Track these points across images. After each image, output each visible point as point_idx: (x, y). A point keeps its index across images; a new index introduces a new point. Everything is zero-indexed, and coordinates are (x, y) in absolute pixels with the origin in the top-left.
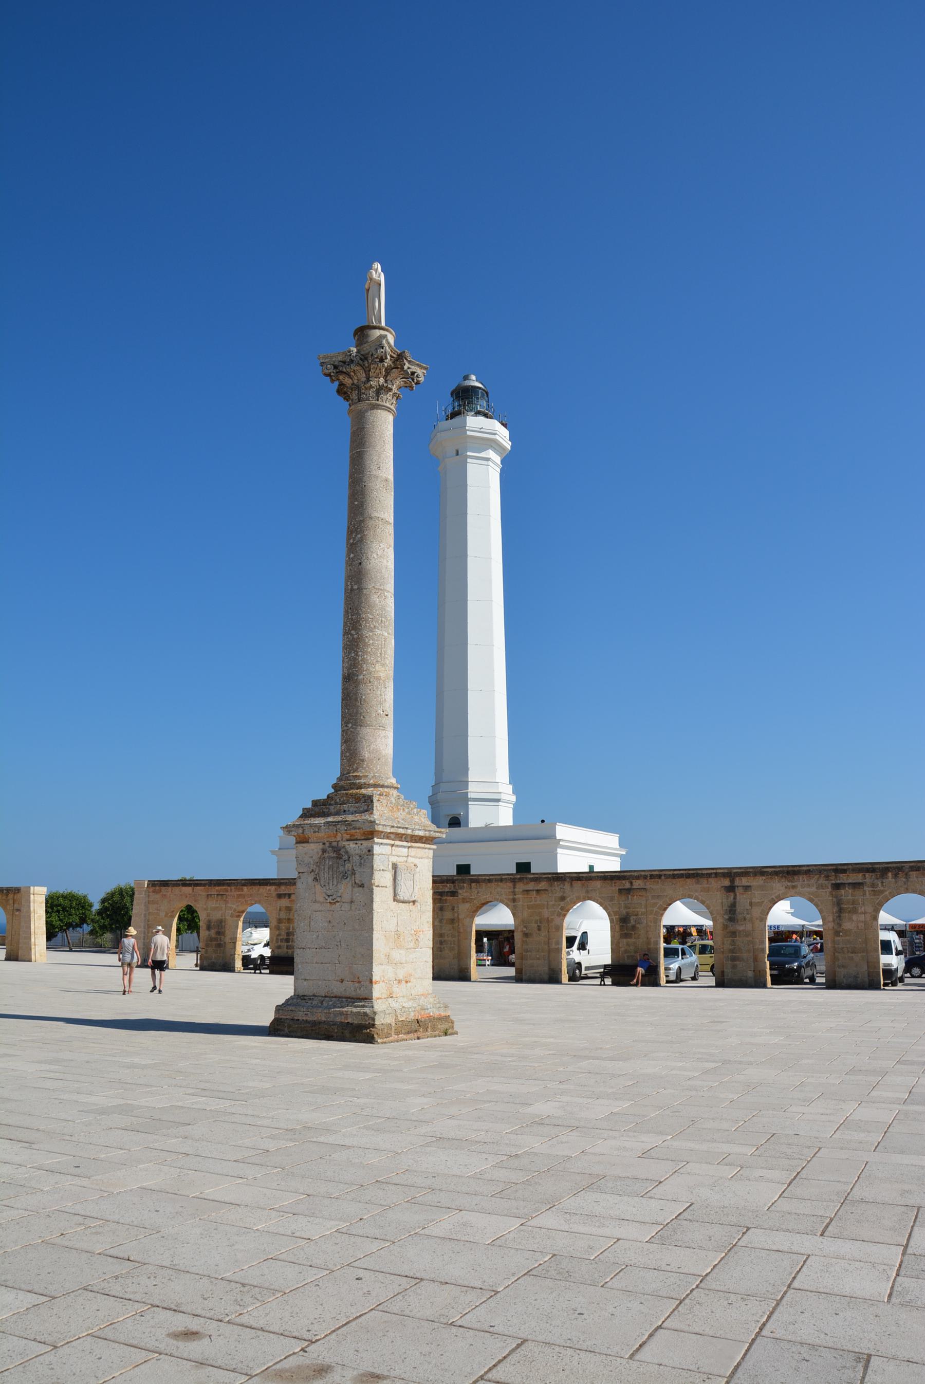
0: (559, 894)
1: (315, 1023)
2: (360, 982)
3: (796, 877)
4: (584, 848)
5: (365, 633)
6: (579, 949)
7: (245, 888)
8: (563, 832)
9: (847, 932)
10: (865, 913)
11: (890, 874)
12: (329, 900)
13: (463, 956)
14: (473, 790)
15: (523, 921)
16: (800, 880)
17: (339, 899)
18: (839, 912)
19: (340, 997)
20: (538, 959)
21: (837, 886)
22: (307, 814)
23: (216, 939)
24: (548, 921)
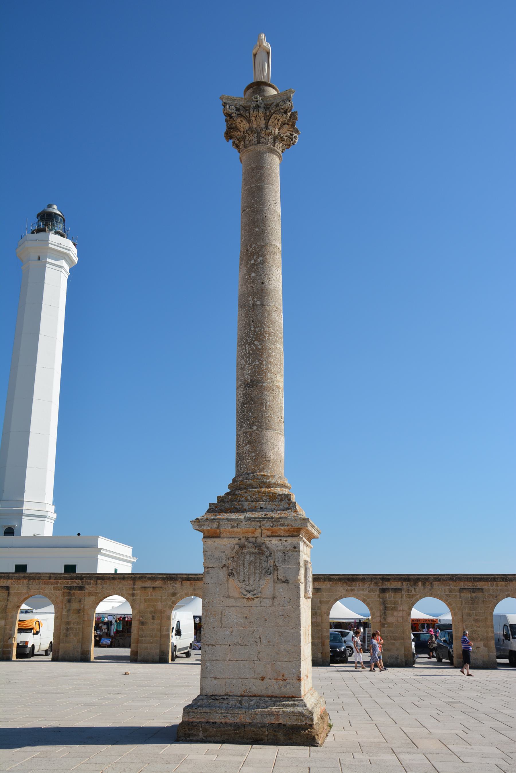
0: (171, 591)
1: (237, 726)
2: (285, 680)
3: (354, 583)
4: (114, 557)
5: (268, 344)
6: (176, 635)
8: (103, 543)
9: (390, 625)
10: (403, 611)
11: (420, 583)
12: (249, 595)
13: (84, 641)
14: (27, 508)
15: (140, 612)
16: (357, 586)
17: (259, 595)
18: (385, 608)
19: (260, 696)
20: (152, 643)
21: (383, 591)
22: (213, 509)
24: (161, 612)
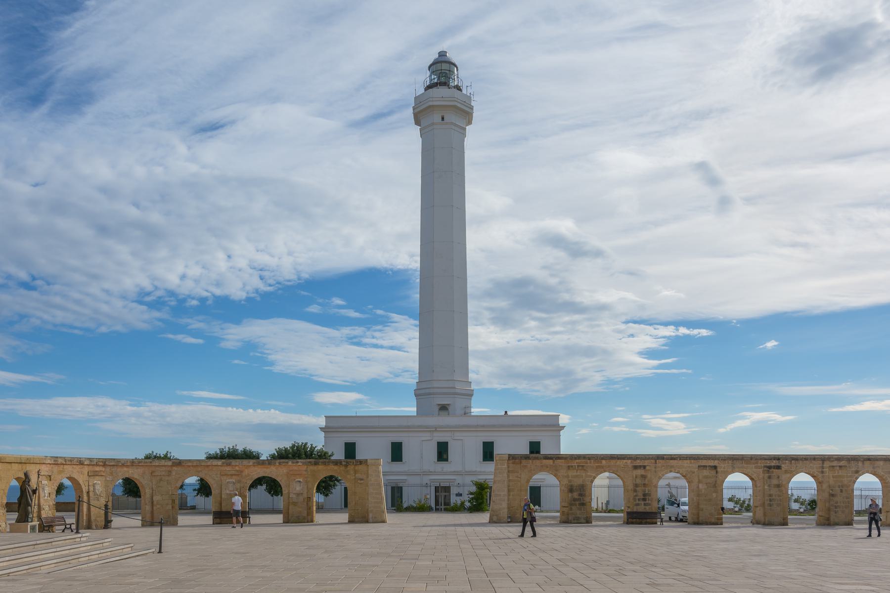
7: (604, 462)
23: (579, 499)
